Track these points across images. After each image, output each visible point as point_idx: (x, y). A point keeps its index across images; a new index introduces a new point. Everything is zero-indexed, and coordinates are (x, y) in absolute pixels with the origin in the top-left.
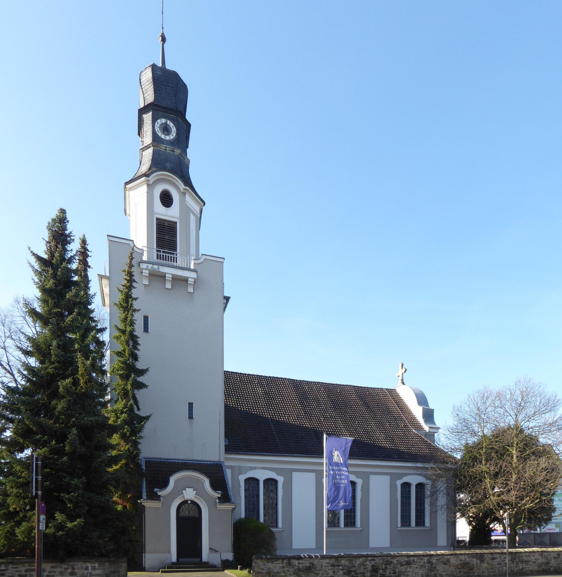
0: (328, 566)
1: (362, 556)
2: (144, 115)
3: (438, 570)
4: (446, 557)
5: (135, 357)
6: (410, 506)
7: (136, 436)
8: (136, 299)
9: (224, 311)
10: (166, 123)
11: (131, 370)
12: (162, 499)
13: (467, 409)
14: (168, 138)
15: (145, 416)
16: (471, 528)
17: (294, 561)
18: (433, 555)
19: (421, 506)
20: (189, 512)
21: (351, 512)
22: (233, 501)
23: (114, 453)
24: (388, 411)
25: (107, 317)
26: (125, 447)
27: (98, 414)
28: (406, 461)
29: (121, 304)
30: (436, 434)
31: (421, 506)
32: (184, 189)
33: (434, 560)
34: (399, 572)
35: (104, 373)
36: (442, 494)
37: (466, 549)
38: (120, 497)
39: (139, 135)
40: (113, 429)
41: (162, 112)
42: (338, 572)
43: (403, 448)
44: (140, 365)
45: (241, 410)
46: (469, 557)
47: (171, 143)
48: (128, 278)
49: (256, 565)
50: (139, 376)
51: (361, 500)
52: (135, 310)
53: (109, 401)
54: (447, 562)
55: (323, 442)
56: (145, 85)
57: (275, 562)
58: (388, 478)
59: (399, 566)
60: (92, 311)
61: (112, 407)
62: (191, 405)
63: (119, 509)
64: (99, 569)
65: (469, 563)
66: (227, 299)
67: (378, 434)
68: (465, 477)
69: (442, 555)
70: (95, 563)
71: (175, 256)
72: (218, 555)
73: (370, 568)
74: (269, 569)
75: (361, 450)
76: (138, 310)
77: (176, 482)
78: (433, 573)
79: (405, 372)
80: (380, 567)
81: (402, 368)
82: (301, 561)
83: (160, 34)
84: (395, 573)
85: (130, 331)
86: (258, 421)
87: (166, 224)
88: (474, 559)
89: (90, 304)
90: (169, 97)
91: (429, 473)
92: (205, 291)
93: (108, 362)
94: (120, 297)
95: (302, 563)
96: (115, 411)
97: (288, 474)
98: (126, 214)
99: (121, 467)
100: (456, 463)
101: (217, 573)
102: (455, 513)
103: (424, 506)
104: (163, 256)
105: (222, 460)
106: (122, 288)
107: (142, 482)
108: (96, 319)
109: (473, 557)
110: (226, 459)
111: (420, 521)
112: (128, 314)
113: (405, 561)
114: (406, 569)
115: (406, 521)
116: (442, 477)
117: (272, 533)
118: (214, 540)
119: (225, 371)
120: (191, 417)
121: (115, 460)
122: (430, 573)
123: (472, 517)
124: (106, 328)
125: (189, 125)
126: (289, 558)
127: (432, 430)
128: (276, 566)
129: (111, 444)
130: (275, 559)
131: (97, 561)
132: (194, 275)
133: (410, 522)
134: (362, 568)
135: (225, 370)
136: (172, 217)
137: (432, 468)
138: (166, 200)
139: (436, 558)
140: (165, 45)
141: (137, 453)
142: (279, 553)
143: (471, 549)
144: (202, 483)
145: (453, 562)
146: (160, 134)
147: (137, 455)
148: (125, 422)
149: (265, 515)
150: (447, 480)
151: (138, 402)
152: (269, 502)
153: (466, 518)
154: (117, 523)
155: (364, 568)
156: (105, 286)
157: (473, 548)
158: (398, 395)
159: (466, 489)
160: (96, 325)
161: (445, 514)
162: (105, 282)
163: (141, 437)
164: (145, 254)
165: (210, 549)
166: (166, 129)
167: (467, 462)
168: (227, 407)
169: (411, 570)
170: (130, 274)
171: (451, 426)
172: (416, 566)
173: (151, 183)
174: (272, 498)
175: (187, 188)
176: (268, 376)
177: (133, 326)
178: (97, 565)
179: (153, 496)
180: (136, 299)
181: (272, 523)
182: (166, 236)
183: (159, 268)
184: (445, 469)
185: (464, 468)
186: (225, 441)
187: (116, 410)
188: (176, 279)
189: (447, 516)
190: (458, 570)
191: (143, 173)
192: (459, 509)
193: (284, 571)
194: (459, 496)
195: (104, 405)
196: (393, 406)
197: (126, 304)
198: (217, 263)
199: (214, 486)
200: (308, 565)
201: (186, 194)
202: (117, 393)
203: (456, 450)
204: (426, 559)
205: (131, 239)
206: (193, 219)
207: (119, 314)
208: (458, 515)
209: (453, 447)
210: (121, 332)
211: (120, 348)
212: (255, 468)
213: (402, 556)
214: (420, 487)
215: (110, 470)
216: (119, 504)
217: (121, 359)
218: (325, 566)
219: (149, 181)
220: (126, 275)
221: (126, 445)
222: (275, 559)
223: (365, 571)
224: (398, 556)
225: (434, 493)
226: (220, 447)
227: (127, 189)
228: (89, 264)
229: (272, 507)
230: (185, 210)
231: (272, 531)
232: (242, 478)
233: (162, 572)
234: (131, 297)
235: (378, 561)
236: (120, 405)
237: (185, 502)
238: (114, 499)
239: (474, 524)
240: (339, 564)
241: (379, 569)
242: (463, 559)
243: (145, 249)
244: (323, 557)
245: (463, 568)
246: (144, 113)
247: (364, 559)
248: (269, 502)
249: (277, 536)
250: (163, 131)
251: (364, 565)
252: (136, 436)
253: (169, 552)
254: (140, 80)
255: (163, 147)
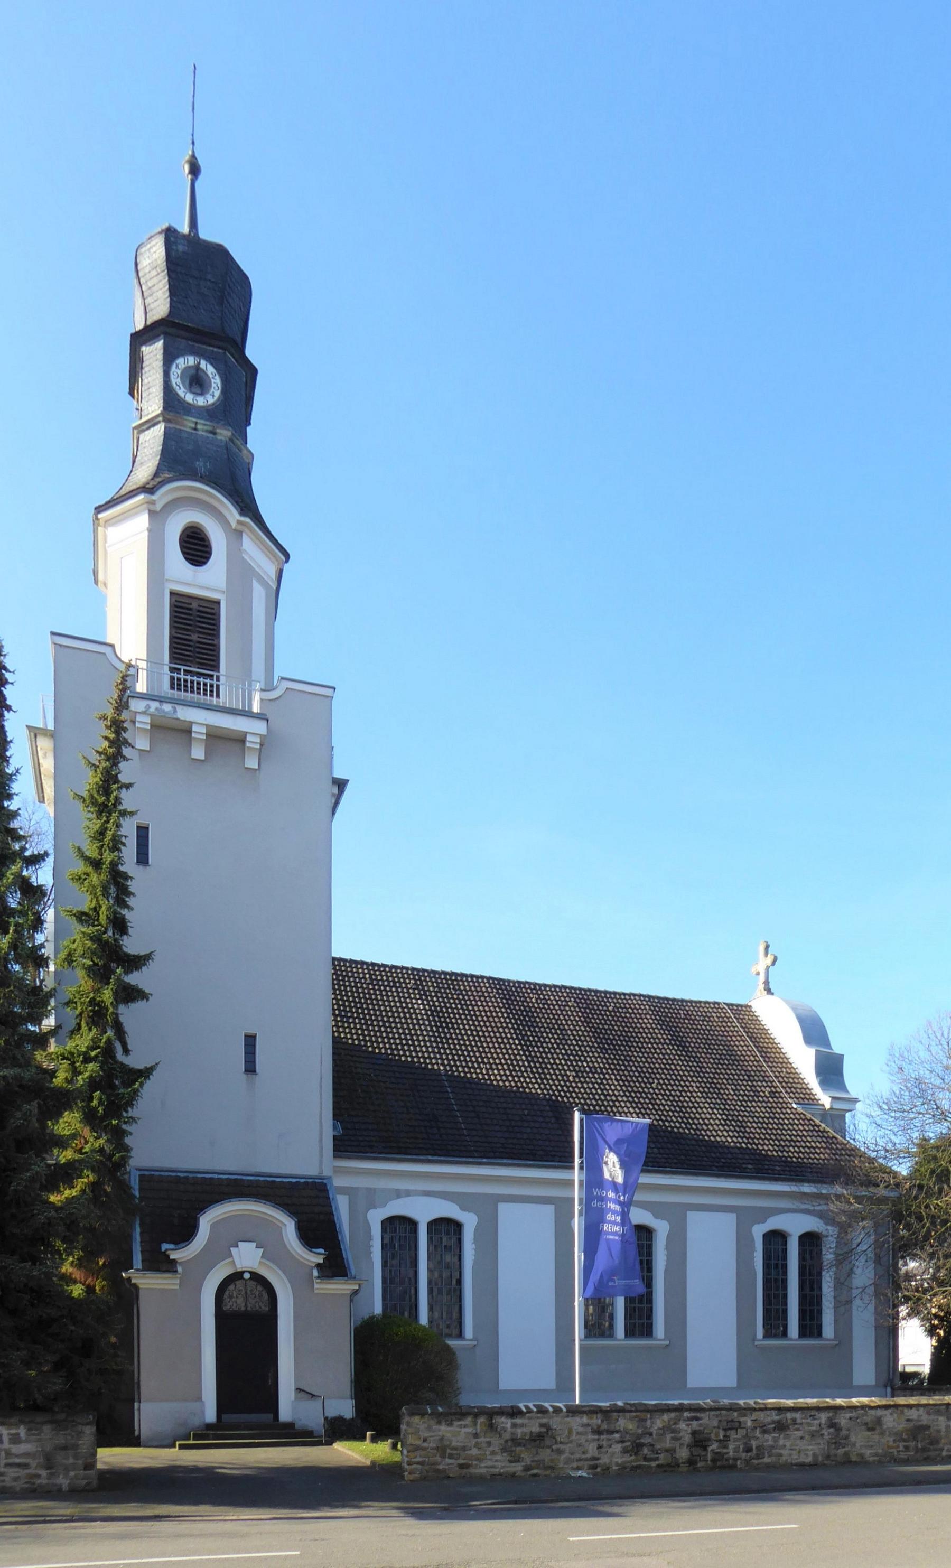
0: (585, 1433)
1: (669, 1409)
2: (144, 348)
3: (854, 1445)
4: (872, 1412)
5: (120, 925)
6: (785, 1288)
7: (119, 1117)
8: (128, 786)
9: (333, 813)
10: (197, 367)
11: (111, 957)
12: (180, 1269)
13: (924, 1054)
14: (200, 401)
15: (141, 1067)
16: (934, 1342)
17: (503, 1419)
18: (840, 1408)
19: (812, 1289)
20: (246, 1299)
21: (641, 1301)
22: (353, 1272)
23: (67, 1155)
24: (731, 1057)
25: (48, 827)
26: (94, 1142)
27: (28, 1062)
28: (776, 1180)
29: (92, 796)
30: (848, 1115)
31: (812, 1289)
32: (239, 522)
33: (843, 1420)
34: (758, 1448)
35: (41, 962)
36: (863, 1259)
37: (922, 1395)
38: (80, 1264)
39: (131, 393)
40: (60, 1101)
41: (187, 339)
42: (610, 1446)
43: (768, 1148)
44: (132, 945)
45: (373, 1052)
46: (928, 1413)
47: (210, 413)
48: (112, 736)
49: (410, 1430)
50: (128, 971)
51: (666, 1271)
52: (124, 813)
53: (54, 1032)
54: (874, 1426)
55: (572, 1130)
56: (148, 277)
57: (456, 1423)
58: (731, 1218)
59: (758, 1433)
60: (14, 815)
61: (61, 1047)
62: (250, 1041)
63: (75, 1294)
64: (27, 1441)
65: (928, 1427)
66: (341, 785)
67: (706, 1111)
68: (920, 1218)
69: (863, 1407)
70: (17, 1425)
71: (215, 682)
72: (316, 1405)
73: (687, 1439)
74: (442, 1439)
75: (670, 1150)
76: (132, 814)
77: (214, 1226)
78: (841, 1451)
79: (774, 963)
80: (713, 1436)
81: (766, 954)
82: (518, 1421)
83: (187, 157)
84: (748, 1450)
85: (111, 863)
86: (417, 1078)
87: (195, 605)
88: (941, 1418)
89: (9, 797)
90: (205, 304)
91: (832, 1207)
92: (289, 767)
93: (51, 938)
94: (89, 781)
95: (522, 1426)
96: (69, 1057)
97: (488, 1209)
98: (96, 582)
99: (83, 1191)
100: (898, 1185)
101: (315, 1448)
102: (895, 1306)
103: (820, 1288)
104: (186, 681)
105: (326, 1173)
106: (95, 758)
107: (132, 1227)
108: (21, 833)
109: (938, 1412)
110: (337, 1170)
111: (811, 1324)
112: (107, 822)
113: (774, 1422)
114: (776, 1440)
115: (775, 1322)
116: (863, 1219)
117: (449, 1350)
118: (309, 1369)
119: (334, 959)
120: (250, 1068)
121: (67, 1174)
122: (833, 1452)
123: (936, 1316)
124: (46, 854)
125: (252, 372)
126: (491, 1414)
127: (838, 1105)
128: (458, 1433)
129: (60, 1136)
130: (455, 1414)
131: (22, 1422)
132: (260, 727)
133: (786, 1327)
134: (669, 1436)
135: (335, 954)
136: (208, 589)
137: (838, 1197)
138: (195, 547)
139: (848, 1415)
140: (198, 184)
141: (123, 1158)
142: (467, 1399)
143: (934, 1394)
144: (278, 1229)
145: (890, 1425)
146: (181, 392)
147: (123, 1161)
148: (93, 1084)
149: (431, 1308)
150: (876, 1226)
151: (124, 1033)
152: (441, 1276)
153: (922, 1320)
154: (73, 1328)
155: (673, 1439)
156: (45, 754)
157: (940, 1390)
158: (755, 1020)
159: (922, 1248)
160: (23, 849)
161: (871, 1308)
162: (44, 744)
163: (133, 1120)
164: (143, 676)
165: (299, 1390)
166: (197, 381)
167: (925, 1182)
168: (339, 1046)
169: (788, 1444)
170: (117, 726)
171: (886, 1094)
172: (799, 1434)
173: (158, 507)
174: (448, 1266)
175: (248, 520)
176: (438, 969)
177: (119, 850)
178: (22, 1431)
179: (159, 1263)
180: (128, 786)
181: (448, 1327)
182: (193, 633)
183: (175, 711)
184: (870, 1198)
185: (916, 1198)
186: (335, 1128)
187: (72, 1054)
188: (215, 737)
189: (876, 1312)
190: (902, 1445)
191: (140, 484)
192: (904, 1296)
193: (477, 1443)
194: (906, 1264)
195: (41, 1040)
196: (744, 1046)
197: (106, 797)
198: (320, 697)
199: (308, 1237)
200: (536, 1429)
201: (244, 536)
202: (77, 1012)
203: (896, 1153)
204: (823, 1417)
205: (108, 641)
206: (259, 595)
207: (85, 821)
208: (903, 1310)
209: (890, 1146)
210: (91, 863)
211: (86, 904)
212: (408, 1193)
213: (765, 1409)
214: (810, 1241)
215: (53, 1198)
216: (75, 1282)
217: (90, 930)
218: (578, 1433)
219: (153, 503)
220: (107, 727)
221: (96, 1138)
222: (455, 1414)
223: (677, 1444)
224: (755, 1409)
225: (845, 1257)
226: (321, 1140)
227: (102, 522)
228: (8, 702)
229: (448, 1287)
230: (241, 572)
231: (448, 1346)
232: (376, 1218)
233: (182, 1447)
234: (116, 781)
235: (708, 1421)
236: (82, 1042)
237: (236, 1276)
238: (63, 1270)
239: (942, 1333)
240: (612, 1428)
241: (709, 1440)
242: (915, 1417)
243: (142, 665)
244: (574, 1411)
245: (915, 1439)
246: (145, 343)
247: (673, 1415)
248: (441, 1276)
249: (461, 1358)
250: (191, 385)
251: (674, 1431)
252: (119, 1117)
253: (199, 1399)
254: (136, 264)
255: (188, 423)
